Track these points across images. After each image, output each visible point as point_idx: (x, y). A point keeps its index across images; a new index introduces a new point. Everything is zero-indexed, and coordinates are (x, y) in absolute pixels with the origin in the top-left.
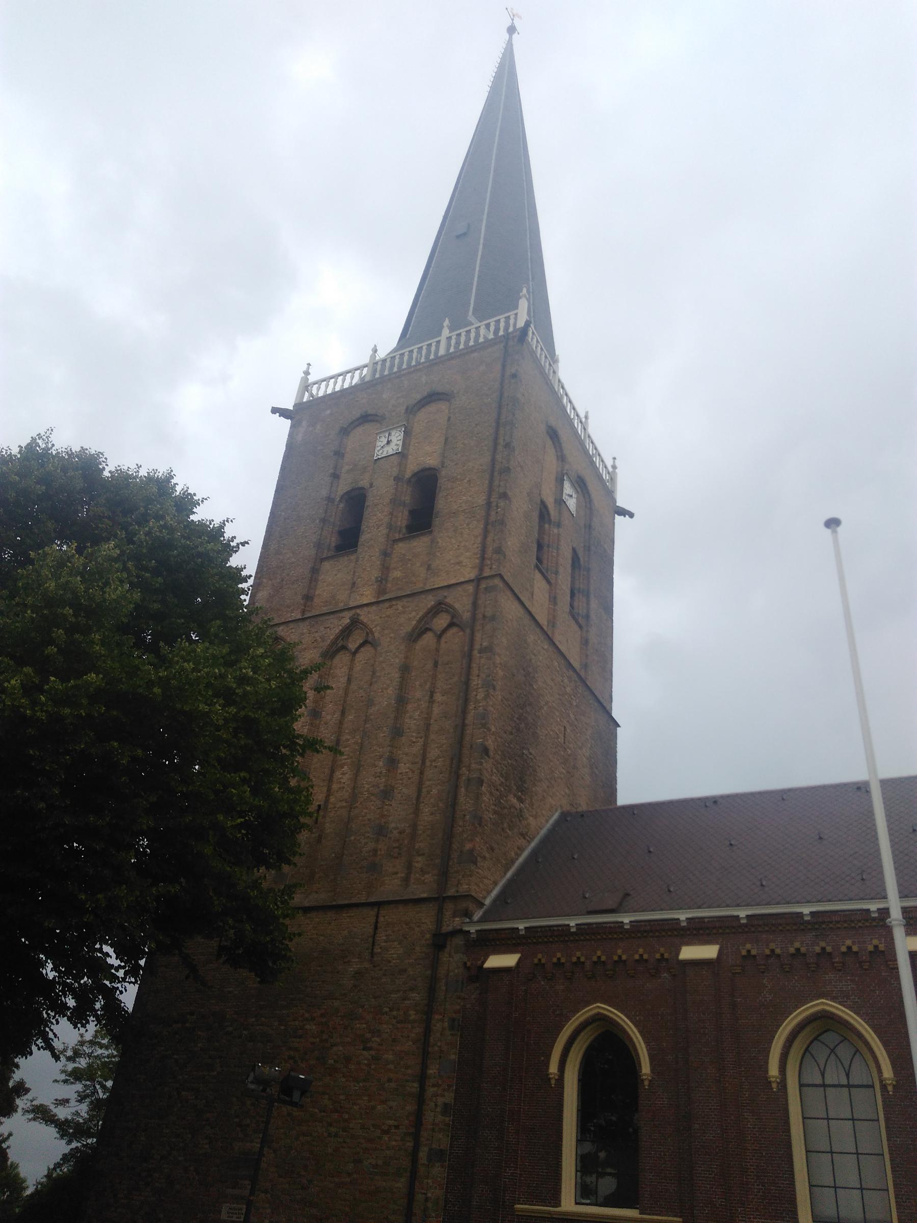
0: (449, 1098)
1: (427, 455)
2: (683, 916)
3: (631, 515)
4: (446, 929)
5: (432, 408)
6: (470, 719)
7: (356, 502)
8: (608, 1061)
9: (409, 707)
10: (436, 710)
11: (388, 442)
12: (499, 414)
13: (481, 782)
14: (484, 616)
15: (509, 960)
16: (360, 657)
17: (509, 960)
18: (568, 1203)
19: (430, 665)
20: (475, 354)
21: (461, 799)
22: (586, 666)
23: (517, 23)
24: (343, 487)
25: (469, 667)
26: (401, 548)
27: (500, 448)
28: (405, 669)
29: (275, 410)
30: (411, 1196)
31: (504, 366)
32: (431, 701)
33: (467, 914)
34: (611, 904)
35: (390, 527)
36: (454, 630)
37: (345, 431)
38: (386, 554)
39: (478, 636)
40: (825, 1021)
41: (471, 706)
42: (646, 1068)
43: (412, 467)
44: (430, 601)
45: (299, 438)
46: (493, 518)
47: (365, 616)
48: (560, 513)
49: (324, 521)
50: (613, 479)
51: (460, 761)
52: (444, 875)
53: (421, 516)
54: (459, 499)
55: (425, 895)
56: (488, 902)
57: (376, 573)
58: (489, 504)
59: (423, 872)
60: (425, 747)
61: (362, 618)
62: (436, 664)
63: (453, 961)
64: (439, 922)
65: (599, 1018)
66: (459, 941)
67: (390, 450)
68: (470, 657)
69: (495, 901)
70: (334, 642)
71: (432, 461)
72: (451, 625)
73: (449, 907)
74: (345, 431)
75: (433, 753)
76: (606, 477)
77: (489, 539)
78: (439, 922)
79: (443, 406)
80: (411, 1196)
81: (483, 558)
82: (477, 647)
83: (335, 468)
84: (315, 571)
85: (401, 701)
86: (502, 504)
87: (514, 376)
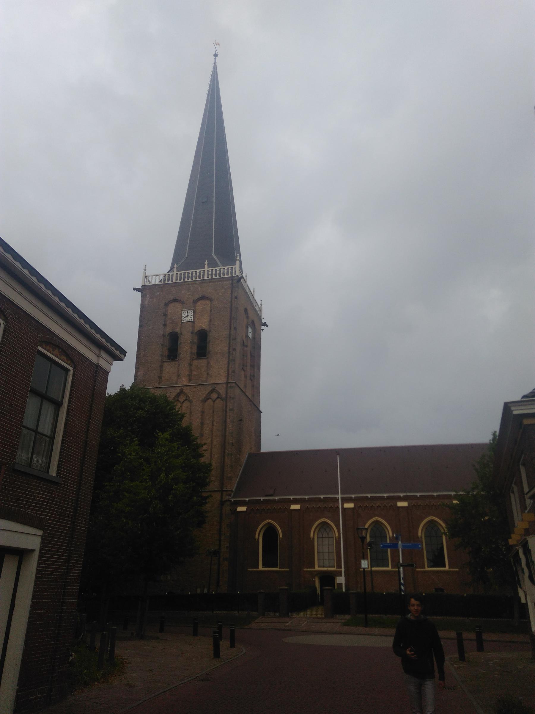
1: (203, 324)
5: (203, 302)
6: (227, 434)
7: (174, 339)
11: (187, 316)
12: (231, 314)
13: (232, 454)
14: (230, 397)
15: (244, 509)
17: (244, 509)
18: (261, 568)
22: (253, 396)
23: (219, 52)
24: (169, 330)
25: (226, 415)
26: (196, 362)
27: (232, 329)
28: (203, 412)
29: (134, 289)
31: (232, 292)
33: (230, 495)
36: (219, 399)
37: (167, 304)
38: (190, 365)
39: (228, 404)
40: (324, 523)
41: (227, 429)
42: (281, 536)
43: (197, 329)
44: (210, 388)
45: (146, 303)
46: (231, 358)
47: (185, 390)
50: (261, 310)
53: (202, 349)
54: (218, 346)
55: (216, 489)
56: (234, 490)
58: (229, 352)
61: (184, 390)
62: (213, 412)
63: (227, 509)
64: (222, 497)
67: (189, 319)
68: (226, 412)
71: (205, 327)
72: (218, 398)
73: (225, 494)
74: (167, 304)
75: (215, 443)
76: (257, 309)
77: (230, 366)
78: (222, 497)
79: (208, 302)
81: (228, 374)
82: (228, 408)
84: (161, 366)
85: (202, 424)
86: (234, 353)
87: (236, 298)
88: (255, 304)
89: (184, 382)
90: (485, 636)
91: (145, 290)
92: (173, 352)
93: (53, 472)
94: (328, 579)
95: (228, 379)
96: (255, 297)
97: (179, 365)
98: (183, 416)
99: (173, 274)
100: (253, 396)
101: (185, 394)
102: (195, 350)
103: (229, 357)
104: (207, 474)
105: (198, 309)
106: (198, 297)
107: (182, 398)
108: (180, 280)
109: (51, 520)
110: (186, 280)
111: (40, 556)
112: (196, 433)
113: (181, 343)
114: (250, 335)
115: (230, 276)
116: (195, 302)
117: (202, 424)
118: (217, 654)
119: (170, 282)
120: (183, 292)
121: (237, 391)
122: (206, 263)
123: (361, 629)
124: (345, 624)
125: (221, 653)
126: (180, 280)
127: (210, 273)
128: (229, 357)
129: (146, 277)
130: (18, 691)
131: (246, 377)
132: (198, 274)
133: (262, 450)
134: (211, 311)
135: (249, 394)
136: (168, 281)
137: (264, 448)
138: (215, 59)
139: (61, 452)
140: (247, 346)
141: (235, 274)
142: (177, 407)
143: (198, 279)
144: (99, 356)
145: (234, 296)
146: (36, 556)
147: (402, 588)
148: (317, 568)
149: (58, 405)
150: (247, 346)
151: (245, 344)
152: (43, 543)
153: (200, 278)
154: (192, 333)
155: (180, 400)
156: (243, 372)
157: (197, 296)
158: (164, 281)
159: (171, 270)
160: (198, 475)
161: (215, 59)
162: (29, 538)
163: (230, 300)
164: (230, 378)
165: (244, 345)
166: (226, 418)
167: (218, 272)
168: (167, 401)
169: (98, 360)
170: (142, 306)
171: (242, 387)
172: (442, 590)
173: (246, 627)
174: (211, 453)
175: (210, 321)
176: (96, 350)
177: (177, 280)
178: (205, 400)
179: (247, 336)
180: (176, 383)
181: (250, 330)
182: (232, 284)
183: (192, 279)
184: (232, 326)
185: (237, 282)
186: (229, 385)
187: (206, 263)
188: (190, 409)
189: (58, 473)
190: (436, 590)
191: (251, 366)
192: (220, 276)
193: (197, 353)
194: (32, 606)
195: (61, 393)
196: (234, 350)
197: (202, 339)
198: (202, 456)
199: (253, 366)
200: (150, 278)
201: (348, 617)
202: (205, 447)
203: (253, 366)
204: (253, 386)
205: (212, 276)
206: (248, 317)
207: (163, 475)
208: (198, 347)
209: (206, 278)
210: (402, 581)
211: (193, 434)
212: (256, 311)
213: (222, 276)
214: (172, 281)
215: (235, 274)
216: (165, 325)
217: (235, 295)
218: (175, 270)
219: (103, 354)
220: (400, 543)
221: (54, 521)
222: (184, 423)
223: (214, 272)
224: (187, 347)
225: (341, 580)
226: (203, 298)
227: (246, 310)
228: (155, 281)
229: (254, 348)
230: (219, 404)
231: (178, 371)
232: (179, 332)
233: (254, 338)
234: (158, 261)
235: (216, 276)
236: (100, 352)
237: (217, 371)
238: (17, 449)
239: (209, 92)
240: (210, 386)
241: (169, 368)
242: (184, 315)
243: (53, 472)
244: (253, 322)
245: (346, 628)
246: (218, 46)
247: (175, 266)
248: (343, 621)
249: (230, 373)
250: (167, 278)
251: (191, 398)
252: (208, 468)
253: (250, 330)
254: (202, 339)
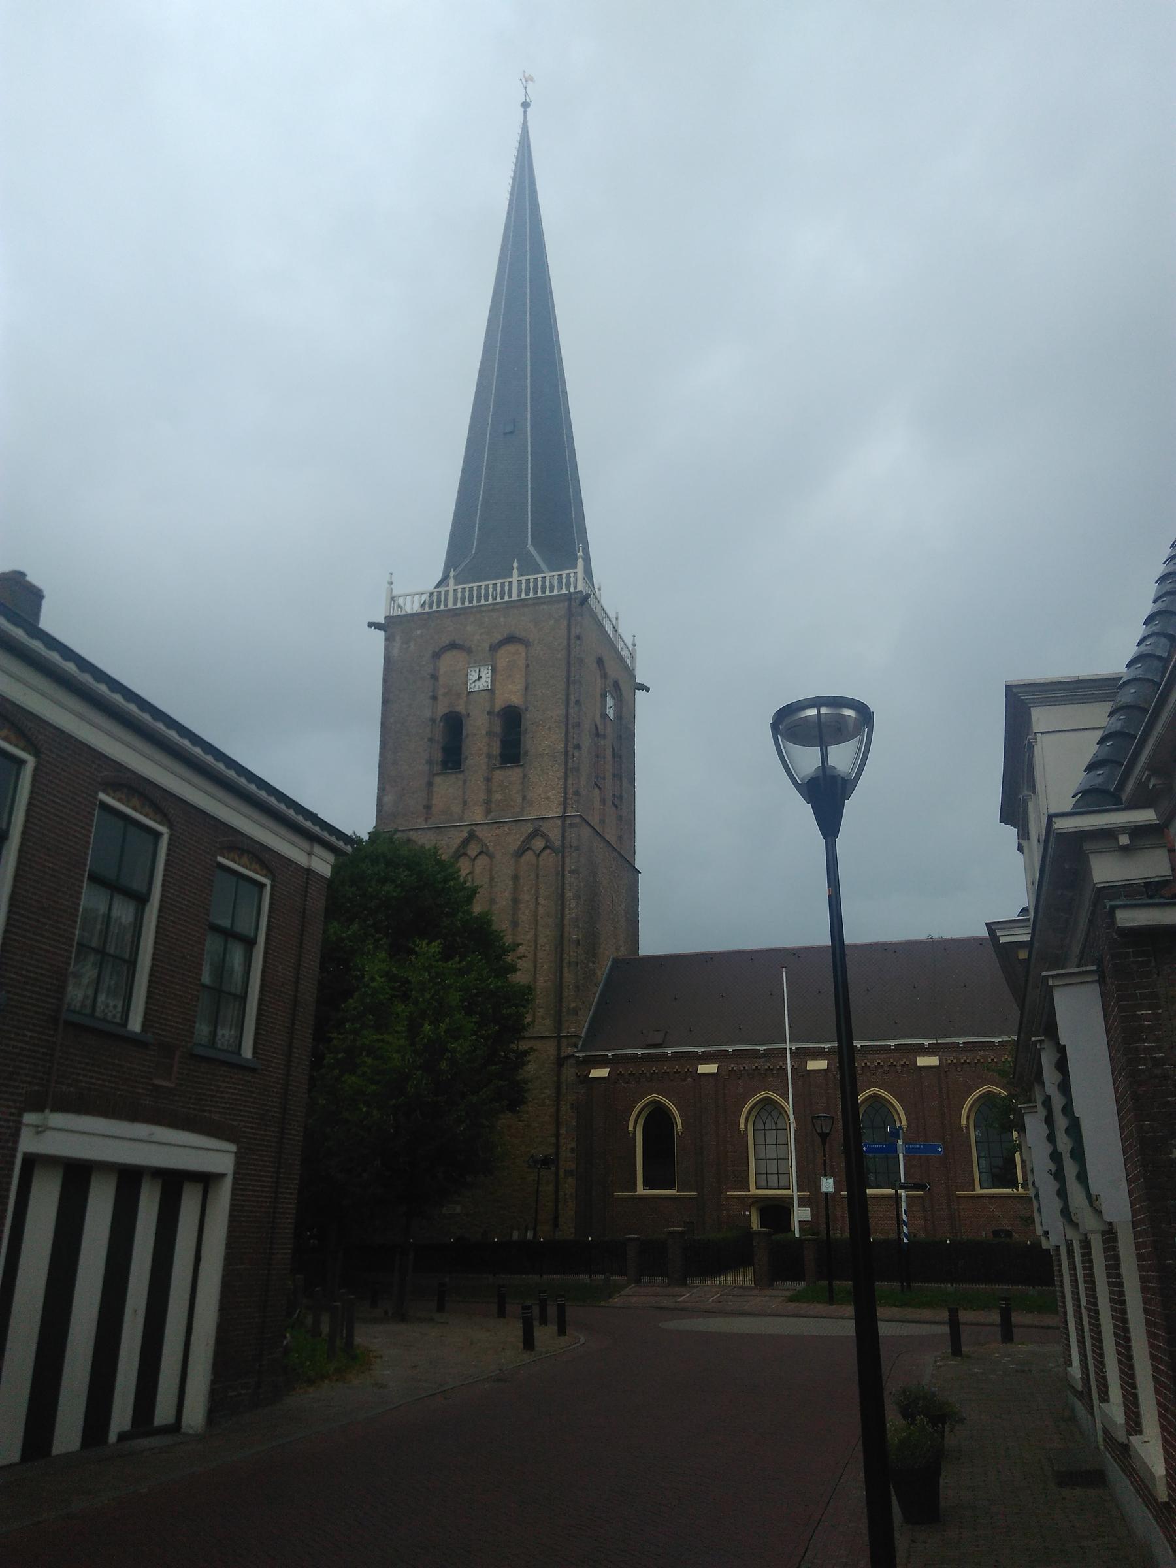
0: (573, 1145)
1: (511, 694)
2: (700, 1050)
3: (648, 690)
4: (563, 1055)
5: (511, 648)
6: (566, 922)
7: (454, 725)
8: (658, 1120)
9: (522, 905)
10: (541, 910)
11: (479, 678)
12: (569, 672)
15: (603, 1072)
16: (478, 862)
17: (603, 1072)
18: (641, 1190)
19: (533, 876)
20: (545, 607)
21: (566, 975)
22: (620, 838)
24: (442, 709)
25: (563, 884)
26: (499, 775)
27: (572, 704)
28: (516, 878)
29: (370, 625)
30: (557, 1192)
32: (537, 904)
33: (575, 1046)
34: (659, 1041)
35: (489, 756)
36: (548, 851)
37: (437, 655)
38: (488, 780)
39: (567, 861)
40: (767, 1100)
41: (567, 912)
42: (680, 1127)
43: (499, 704)
44: (530, 828)
45: (395, 652)
46: (570, 765)
48: (605, 724)
49: (431, 740)
50: (632, 657)
51: (562, 950)
52: (559, 1023)
53: (511, 746)
54: (543, 740)
55: (547, 1034)
57: (482, 796)
58: (567, 752)
59: (543, 1019)
60: (536, 935)
62: (537, 877)
63: (569, 1073)
64: (559, 1050)
65: (655, 1102)
66: (572, 1061)
68: (563, 876)
69: (587, 1033)
70: (457, 850)
71: (516, 700)
73: (564, 1042)
74: (437, 655)
77: (570, 782)
78: (559, 1050)
79: (521, 648)
80: (557, 1192)
81: (565, 798)
82: (567, 869)
83: (433, 691)
84: (430, 784)
85: (516, 901)
86: (576, 754)
87: (578, 638)
88: (620, 646)
89: (477, 815)
90: (1017, 1318)
92: (452, 756)
93: (247, 1052)
94: (776, 1212)
95: (565, 808)
96: (620, 631)
97: (465, 782)
98: (474, 891)
99: (447, 592)
100: (620, 838)
101: (479, 840)
102: (496, 750)
103: (566, 763)
104: (524, 1007)
106: (500, 637)
107: (473, 850)
108: (463, 603)
109: (246, 1127)
110: (475, 603)
111: (234, 1184)
112: (501, 923)
113: (468, 735)
114: (611, 713)
115: (564, 591)
116: (494, 648)
117: (516, 901)
118: (529, 1343)
119: (442, 607)
120: (469, 628)
121: (586, 832)
122: (515, 565)
123: (820, 1308)
124: (791, 1299)
125: (536, 1343)
126: (463, 603)
127: (524, 586)
128: (566, 763)
129: (393, 599)
130: (213, 1382)
131: (603, 801)
132: (499, 589)
133: (642, 953)
134: (527, 666)
135: (611, 837)
136: (439, 605)
137: (647, 948)
138: (525, 112)
139: (258, 1019)
140: (604, 737)
141: (575, 588)
142: (463, 873)
143: (498, 600)
144: (310, 854)
145: (573, 636)
146: (228, 1184)
147: (905, 1229)
148: (753, 1191)
149: (250, 943)
150: (604, 737)
151: (601, 731)
152: (238, 1164)
153: (502, 598)
154: (489, 713)
155: (469, 852)
156: (597, 791)
157: (498, 637)
158: (431, 606)
159: (443, 582)
160: (502, 1012)
161: (525, 112)
162: (214, 1156)
163: (565, 643)
164: (569, 808)
165: (598, 735)
166: (563, 889)
167: (540, 584)
168: (439, 862)
169: (310, 862)
170: (388, 660)
171: (595, 822)
172: (1009, 1234)
173: (603, 1304)
174: (535, 962)
175: (526, 688)
176: (306, 845)
177: (455, 603)
179: (604, 716)
180: (461, 819)
181: (610, 702)
182: (570, 608)
183: (486, 600)
184: (572, 697)
185: (580, 605)
186: (568, 822)
187: (515, 565)
188: (491, 870)
189: (255, 1053)
190: (996, 1233)
191: (614, 775)
192: (544, 591)
193: (501, 755)
194: (226, 1259)
195: (253, 925)
196: (578, 747)
197: (511, 722)
198: (513, 969)
199: (617, 776)
200: (401, 601)
201: (800, 1286)
202: (522, 949)
203: (617, 776)
204: (620, 818)
205: (527, 594)
206: (604, 676)
207: (427, 1027)
208: (502, 741)
209: (515, 597)
210: (904, 1217)
211: (494, 927)
212: (621, 659)
213: (548, 593)
214: (446, 605)
215: (575, 588)
216: (434, 698)
217: (576, 631)
218: (452, 581)
219: (318, 849)
220: (900, 1142)
221: (252, 1128)
222: (477, 909)
223: (531, 585)
224: (480, 742)
225: (801, 1214)
226: (511, 639)
227: (600, 662)
228: (412, 606)
229: (619, 737)
230: (549, 858)
231: (464, 793)
232: (463, 712)
233: (619, 717)
234: (416, 563)
235: (535, 593)
236: (312, 848)
237: (543, 791)
238: (194, 1022)
239: (513, 187)
240: (529, 824)
241: (446, 788)
242: (473, 676)
243: (247, 1052)
244: (616, 685)
245: (792, 1306)
246: (530, 84)
247: (452, 574)
248: (788, 1293)
249: (570, 796)
250: (435, 598)
251: (491, 849)
252: (524, 995)
253: (610, 702)
254: (511, 722)
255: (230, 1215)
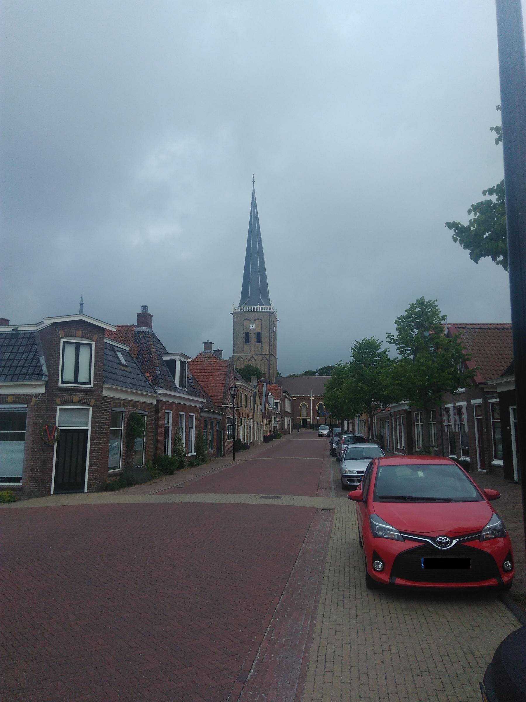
1: (259, 330)
7: (247, 335)
37: (243, 321)
47: (254, 356)
54: (265, 339)
67: (253, 328)
71: (260, 331)
74: (243, 321)
91: (234, 314)
94: (304, 420)
105: (257, 323)
178: (261, 360)
197: (259, 334)
226: (258, 319)
241: (246, 347)
254: (259, 334)
255: (193, 503)
